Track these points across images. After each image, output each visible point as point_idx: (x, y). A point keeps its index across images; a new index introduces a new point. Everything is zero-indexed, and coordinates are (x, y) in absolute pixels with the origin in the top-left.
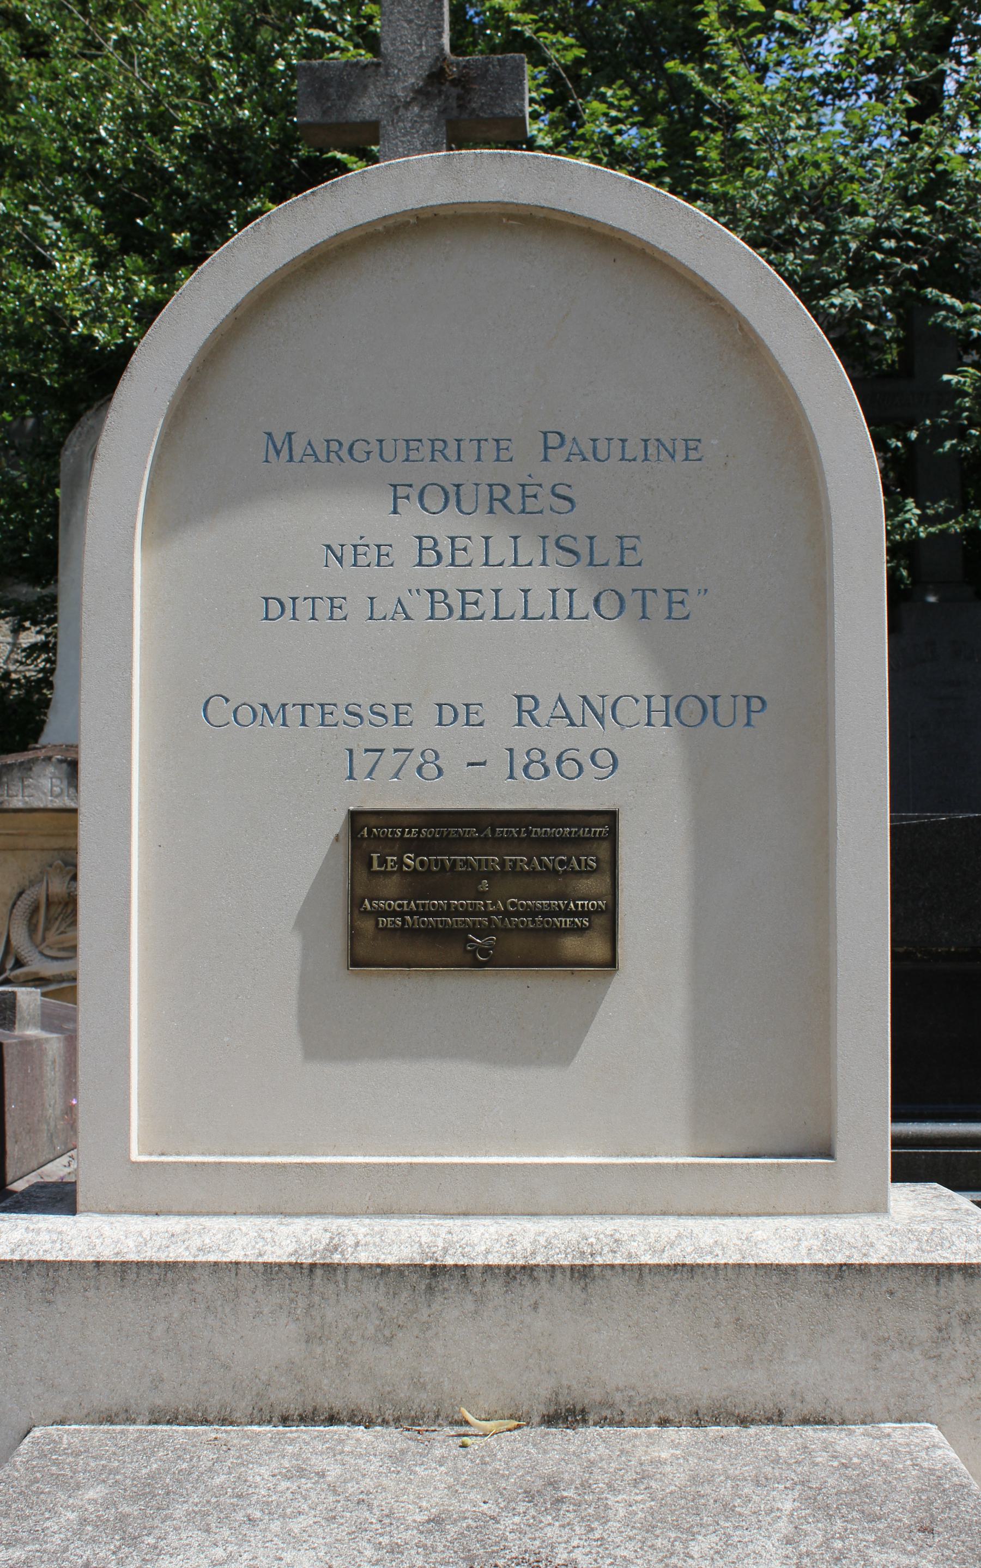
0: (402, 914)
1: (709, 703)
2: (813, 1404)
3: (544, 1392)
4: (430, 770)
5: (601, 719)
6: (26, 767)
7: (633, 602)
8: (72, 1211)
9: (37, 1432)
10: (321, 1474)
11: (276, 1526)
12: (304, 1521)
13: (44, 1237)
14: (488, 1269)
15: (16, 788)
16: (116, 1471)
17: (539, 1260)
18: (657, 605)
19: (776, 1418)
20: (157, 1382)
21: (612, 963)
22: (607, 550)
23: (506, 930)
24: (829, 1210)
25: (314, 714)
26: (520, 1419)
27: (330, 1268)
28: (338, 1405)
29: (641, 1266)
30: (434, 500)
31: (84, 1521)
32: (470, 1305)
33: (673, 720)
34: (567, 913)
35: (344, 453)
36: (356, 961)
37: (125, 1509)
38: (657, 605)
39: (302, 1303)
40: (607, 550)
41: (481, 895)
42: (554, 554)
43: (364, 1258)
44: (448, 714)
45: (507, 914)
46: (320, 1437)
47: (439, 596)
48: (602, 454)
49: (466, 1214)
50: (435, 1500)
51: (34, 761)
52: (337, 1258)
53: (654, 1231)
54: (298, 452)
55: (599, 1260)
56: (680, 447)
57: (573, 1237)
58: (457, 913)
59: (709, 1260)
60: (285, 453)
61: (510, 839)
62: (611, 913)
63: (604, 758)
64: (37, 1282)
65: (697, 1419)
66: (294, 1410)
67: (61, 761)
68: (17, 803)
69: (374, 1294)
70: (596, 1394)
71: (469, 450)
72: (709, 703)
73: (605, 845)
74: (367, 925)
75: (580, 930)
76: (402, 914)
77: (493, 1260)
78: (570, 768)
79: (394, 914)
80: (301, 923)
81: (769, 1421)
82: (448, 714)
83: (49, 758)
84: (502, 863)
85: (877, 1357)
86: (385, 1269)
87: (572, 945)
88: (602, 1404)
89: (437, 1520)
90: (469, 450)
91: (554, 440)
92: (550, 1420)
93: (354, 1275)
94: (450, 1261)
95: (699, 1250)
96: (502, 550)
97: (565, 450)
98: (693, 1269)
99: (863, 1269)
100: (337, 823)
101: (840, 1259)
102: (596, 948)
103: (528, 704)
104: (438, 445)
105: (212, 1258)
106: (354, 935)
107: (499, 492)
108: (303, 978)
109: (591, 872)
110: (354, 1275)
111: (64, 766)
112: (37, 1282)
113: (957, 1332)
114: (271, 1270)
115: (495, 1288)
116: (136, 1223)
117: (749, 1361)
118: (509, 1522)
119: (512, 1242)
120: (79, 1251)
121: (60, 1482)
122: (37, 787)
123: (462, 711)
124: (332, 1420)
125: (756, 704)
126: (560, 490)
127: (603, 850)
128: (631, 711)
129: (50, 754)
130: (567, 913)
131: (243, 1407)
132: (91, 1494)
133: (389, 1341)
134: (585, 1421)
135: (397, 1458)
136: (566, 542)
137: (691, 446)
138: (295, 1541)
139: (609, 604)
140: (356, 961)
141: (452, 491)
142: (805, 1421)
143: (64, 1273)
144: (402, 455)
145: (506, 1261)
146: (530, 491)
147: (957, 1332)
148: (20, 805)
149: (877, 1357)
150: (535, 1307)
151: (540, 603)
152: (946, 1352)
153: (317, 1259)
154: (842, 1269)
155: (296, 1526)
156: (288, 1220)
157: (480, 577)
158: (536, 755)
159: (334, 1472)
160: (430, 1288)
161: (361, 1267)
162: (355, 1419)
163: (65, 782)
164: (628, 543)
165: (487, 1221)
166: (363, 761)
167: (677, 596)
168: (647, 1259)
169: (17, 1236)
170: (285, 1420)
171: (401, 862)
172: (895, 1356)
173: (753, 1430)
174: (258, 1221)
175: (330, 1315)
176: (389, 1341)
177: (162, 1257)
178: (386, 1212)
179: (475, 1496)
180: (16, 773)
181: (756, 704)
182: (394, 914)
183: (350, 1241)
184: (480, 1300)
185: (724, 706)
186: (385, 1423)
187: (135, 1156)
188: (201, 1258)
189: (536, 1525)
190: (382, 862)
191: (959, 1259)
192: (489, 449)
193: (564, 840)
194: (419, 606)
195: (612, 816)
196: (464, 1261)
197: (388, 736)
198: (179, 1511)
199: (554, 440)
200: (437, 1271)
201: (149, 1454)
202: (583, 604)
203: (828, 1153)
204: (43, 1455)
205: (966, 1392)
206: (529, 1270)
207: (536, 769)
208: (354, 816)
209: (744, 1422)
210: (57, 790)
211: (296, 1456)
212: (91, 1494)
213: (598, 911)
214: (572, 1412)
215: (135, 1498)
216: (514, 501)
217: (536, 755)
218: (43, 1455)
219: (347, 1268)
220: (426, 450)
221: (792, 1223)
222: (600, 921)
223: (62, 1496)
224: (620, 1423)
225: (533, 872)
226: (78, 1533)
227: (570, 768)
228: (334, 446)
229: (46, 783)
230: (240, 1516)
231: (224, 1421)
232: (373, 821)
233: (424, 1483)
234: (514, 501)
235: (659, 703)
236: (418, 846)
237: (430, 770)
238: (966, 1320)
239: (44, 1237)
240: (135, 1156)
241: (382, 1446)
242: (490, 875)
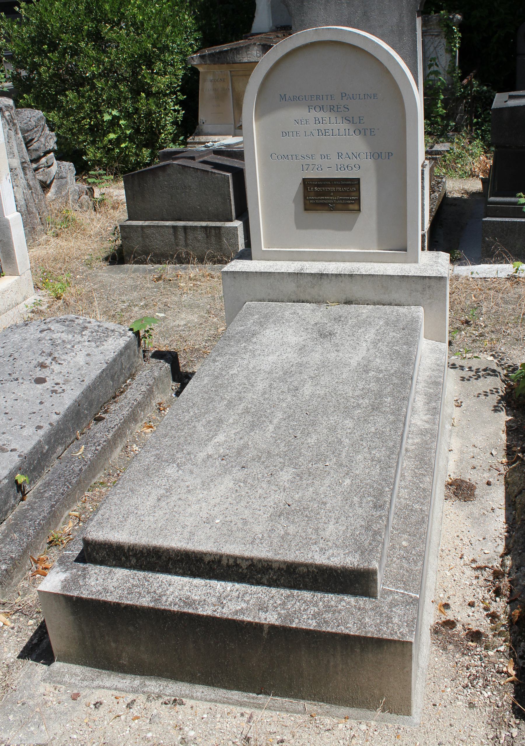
0: (315, 200)
1: (380, 154)
2: (398, 302)
3: (344, 298)
4: (320, 169)
5: (356, 158)
6: (247, 47)
7: (363, 132)
8: (252, 260)
9: (247, 303)
10: (298, 314)
11: (287, 324)
12: (292, 323)
13: (246, 266)
14: (332, 274)
15: (245, 55)
16: (260, 312)
17: (342, 273)
18: (368, 132)
19: (390, 304)
20: (269, 294)
21: (359, 210)
22: (356, 120)
23: (337, 203)
24: (405, 262)
25: (294, 157)
26: (339, 303)
27: (301, 274)
28: (304, 299)
29: (362, 275)
30: (318, 109)
31: (254, 322)
32: (329, 281)
33: (372, 158)
34: (350, 200)
35: (297, 99)
36: (306, 209)
37: (261, 320)
38: (368, 132)
39: (296, 280)
40: (356, 120)
41: (331, 196)
42: (344, 121)
43: (308, 272)
44: (323, 157)
45: (337, 200)
46: (300, 306)
47: (320, 131)
48: (355, 98)
49: (330, 261)
50: (317, 319)
51: (250, 45)
52: (302, 272)
53: (367, 267)
54: (287, 99)
55: (354, 273)
56: (372, 96)
57: (350, 268)
58: (327, 200)
59: (376, 274)
60: (284, 99)
61: (337, 184)
62: (359, 199)
63: (357, 166)
64: (245, 275)
65: (374, 304)
66: (296, 300)
67: (259, 45)
68: (245, 60)
69: (310, 279)
70: (354, 299)
71: (325, 98)
72: (380, 154)
73: (357, 186)
74: (308, 202)
75: (353, 203)
76: (315, 200)
77: (333, 273)
78: (350, 168)
79: (313, 200)
80: (294, 201)
81: (389, 305)
82: (323, 157)
83: (255, 44)
84: (335, 189)
85: (411, 293)
86: (312, 274)
87: (351, 207)
88: (356, 300)
89: (316, 324)
90: (325, 98)
91: (344, 95)
92: (345, 303)
93: (306, 275)
94: (325, 273)
95: (375, 271)
96: (333, 120)
97: (346, 97)
98: (373, 275)
99: (408, 277)
100: (300, 181)
101: (403, 274)
102: (356, 207)
103: (340, 154)
104: (318, 97)
105: (278, 271)
106: (305, 204)
107: (332, 107)
108: (295, 213)
109: (354, 191)
110: (306, 275)
111: (260, 46)
112: (245, 275)
113: (427, 289)
114: (289, 274)
115: (334, 278)
116: (263, 262)
117: (385, 293)
118: (329, 324)
119: (337, 269)
120: (252, 270)
121: (250, 314)
122: (251, 54)
123: (326, 156)
124: (303, 302)
125: (390, 154)
126: (345, 106)
127: (357, 186)
128: (363, 156)
129: (255, 42)
130: (350, 200)
131: (286, 299)
132: (256, 317)
133: (313, 287)
134: (352, 304)
135: (313, 311)
136: (347, 118)
137: (375, 95)
138: (290, 327)
139: (357, 132)
140: (306, 209)
141: (321, 107)
142: (396, 305)
143: (250, 274)
144: (310, 99)
145: (336, 273)
146: (339, 107)
147: (427, 289)
148: (246, 61)
149: (411, 293)
150: (342, 282)
151: (342, 132)
152: (425, 293)
153: (298, 272)
154: (403, 276)
155: (291, 324)
156: (294, 262)
157: (328, 126)
158: (342, 165)
159: (301, 313)
160: (321, 278)
161: (307, 273)
162: (307, 302)
163: (261, 52)
164: (361, 118)
165: (334, 263)
166: (305, 167)
167: (372, 130)
168: (364, 273)
169: (240, 266)
170: (294, 302)
171: (314, 189)
172: (414, 293)
173: (385, 306)
174: (288, 262)
175: (301, 282)
176: (313, 287)
177: (268, 271)
178: (314, 260)
179: (325, 319)
180: (244, 50)
181: (390, 154)
182: (313, 200)
183: (305, 268)
184: (331, 280)
185: (383, 155)
186: (313, 303)
187: (263, 249)
188: (276, 271)
189: (333, 325)
190: (310, 189)
191: (428, 275)
192: (329, 97)
193: (348, 184)
194: (315, 133)
195: (358, 180)
196: (327, 273)
197: (309, 161)
198: (271, 321)
199: (344, 95)
200: (322, 275)
201: (267, 308)
202: (352, 132)
203: (406, 250)
204: (248, 308)
205: (429, 301)
206: (340, 275)
207: (342, 169)
208: (304, 180)
209: (384, 305)
210: (258, 55)
211: (294, 310)
212: (256, 317)
213: (356, 199)
214: (349, 302)
215: (263, 318)
216: (335, 109)
217: (342, 165)
218: (248, 308)
219: (304, 273)
220: (315, 98)
221: (396, 265)
222: (357, 201)
223: (251, 317)
224: (359, 304)
225: (342, 191)
226: (253, 324)
227: (350, 168)
228: (295, 97)
229: (255, 53)
230: (281, 322)
231: (282, 302)
232: (308, 180)
233: (317, 316)
234: (335, 109)
235: (369, 154)
236: (318, 186)
237: (320, 169)
238: (429, 287)
239: (246, 266)
240: (263, 249)
241: (311, 308)
242: (333, 192)
